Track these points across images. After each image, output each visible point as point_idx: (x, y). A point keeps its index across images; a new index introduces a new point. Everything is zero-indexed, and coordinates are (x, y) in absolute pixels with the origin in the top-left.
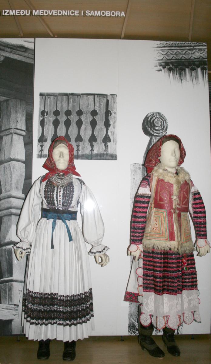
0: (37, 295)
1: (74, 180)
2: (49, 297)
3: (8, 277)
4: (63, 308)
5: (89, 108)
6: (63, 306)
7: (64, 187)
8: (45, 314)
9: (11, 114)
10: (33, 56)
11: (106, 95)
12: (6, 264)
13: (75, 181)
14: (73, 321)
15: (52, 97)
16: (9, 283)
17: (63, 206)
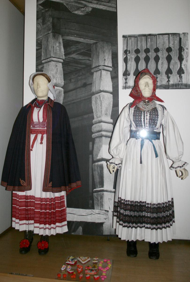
0: (129, 203)
1: (157, 106)
2: (139, 204)
3: (100, 188)
4: (151, 214)
5: (165, 45)
6: (150, 212)
7: (149, 112)
8: (134, 219)
9: (100, 54)
10: (115, 6)
11: (179, 34)
12: (98, 177)
13: (158, 106)
14: (158, 225)
15: (133, 38)
16: (101, 193)
17: (149, 128)
